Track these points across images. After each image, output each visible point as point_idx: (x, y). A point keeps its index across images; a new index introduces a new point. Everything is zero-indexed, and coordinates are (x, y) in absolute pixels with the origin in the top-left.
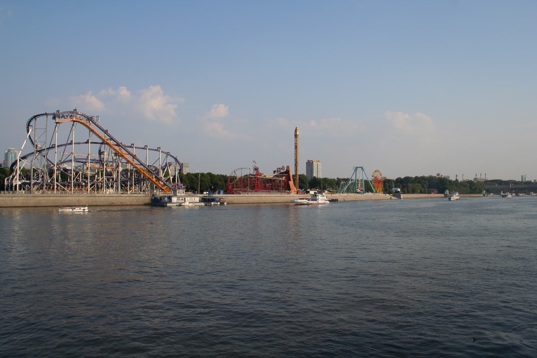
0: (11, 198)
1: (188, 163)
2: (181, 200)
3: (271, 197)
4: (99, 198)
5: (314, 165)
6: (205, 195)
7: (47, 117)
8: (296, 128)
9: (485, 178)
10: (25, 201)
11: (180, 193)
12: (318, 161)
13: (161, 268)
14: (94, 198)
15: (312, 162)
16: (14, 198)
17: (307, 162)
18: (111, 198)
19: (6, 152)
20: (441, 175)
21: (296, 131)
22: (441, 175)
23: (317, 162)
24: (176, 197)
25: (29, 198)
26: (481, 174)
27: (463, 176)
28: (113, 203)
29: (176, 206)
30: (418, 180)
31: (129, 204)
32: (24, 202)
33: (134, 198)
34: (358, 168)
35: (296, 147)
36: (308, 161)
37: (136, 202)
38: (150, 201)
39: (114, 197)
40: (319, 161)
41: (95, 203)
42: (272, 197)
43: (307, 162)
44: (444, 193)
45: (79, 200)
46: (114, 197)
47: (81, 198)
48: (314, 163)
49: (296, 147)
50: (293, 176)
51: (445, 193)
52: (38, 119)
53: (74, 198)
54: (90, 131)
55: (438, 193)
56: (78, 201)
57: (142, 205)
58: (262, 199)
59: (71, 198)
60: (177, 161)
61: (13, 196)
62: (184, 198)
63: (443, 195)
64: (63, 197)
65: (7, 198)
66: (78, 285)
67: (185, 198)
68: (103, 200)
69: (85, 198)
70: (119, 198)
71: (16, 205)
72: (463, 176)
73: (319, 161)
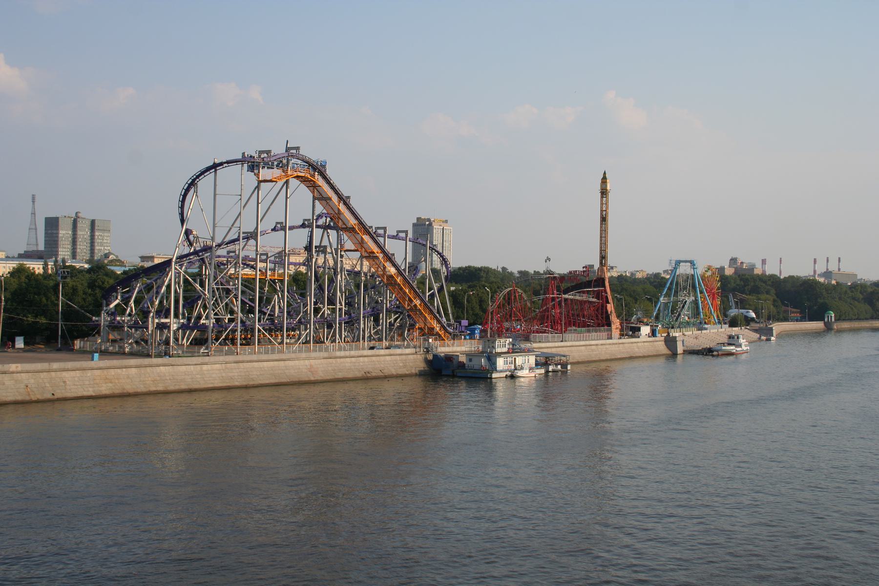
1: (110, 221)
3: (605, 347)
5: (434, 231)
8: (605, 173)
9: (839, 270)
10: (224, 375)
12: (443, 222)
13: (633, 520)
15: (430, 224)
16: (205, 367)
17: (415, 221)
20: (740, 262)
21: (604, 180)
22: (742, 263)
23: (442, 224)
25: (228, 365)
26: (828, 258)
27: (781, 263)
30: (752, 284)
32: (223, 377)
33: (398, 357)
34: (682, 264)
35: (604, 219)
36: (418, 219)
38: (425, 366)
39: (365, 356)
40: (446, 221)
41: (340, 374)
42: (607, 346)
43: (415, 221)
44: (824, 321)
45: (311, 366)
46: (365, 356)
47: (313, 362)
48: (436, 227)
49: (604, 219)
50: (316, 247)
51: (826, 320)
52: (221, 171)
53: (302, 362)
54: (314, 198)
55: (803, 319)
58: (593, 351)
59: (297, 362)
60: (446, 262)
61: (202, 361)
62: (513, 358)
63: (819, 325)
64: (284, 360)
66: (544, 568)
68: (349, 364)
69: (319, 361)
70: (374, 358)
71: (212, 383)
72: (781, 263)
73: (446, 221)
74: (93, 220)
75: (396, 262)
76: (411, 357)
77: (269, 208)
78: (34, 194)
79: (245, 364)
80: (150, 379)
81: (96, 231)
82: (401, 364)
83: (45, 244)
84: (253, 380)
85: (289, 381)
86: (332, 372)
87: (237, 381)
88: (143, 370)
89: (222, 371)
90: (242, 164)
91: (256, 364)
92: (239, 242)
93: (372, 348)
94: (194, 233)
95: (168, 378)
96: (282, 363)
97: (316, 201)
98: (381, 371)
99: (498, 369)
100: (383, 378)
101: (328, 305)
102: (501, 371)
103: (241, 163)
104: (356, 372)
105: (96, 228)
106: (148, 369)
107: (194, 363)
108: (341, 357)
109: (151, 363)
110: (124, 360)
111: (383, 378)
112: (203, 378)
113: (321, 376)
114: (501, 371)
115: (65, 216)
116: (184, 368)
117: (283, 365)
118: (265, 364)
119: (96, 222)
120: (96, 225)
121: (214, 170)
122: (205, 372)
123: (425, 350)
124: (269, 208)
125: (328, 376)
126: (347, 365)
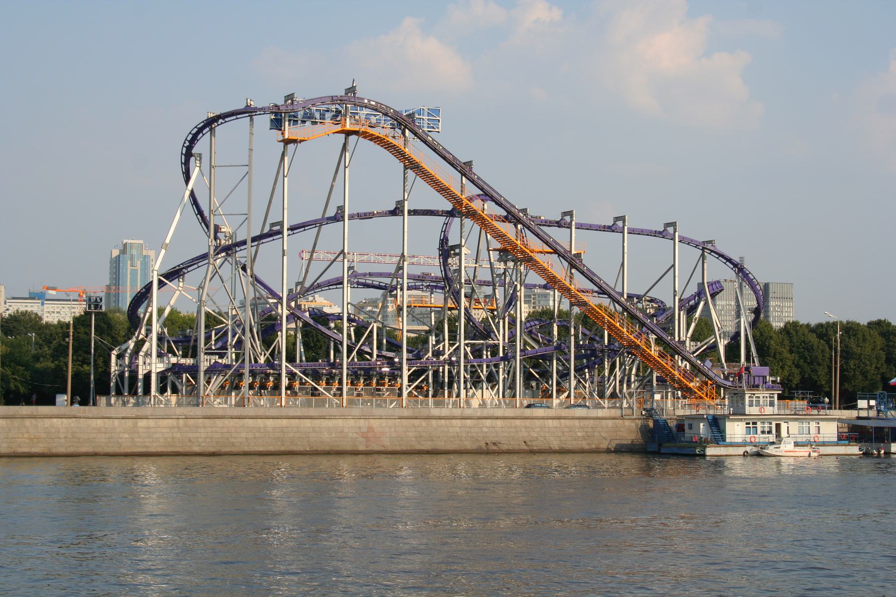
0: (130, 423)
2: (763, 432)
4: (443, 422)
6: (864, 414)
7: (252, 120)
11: (758, 404)
14: (424, 423)
16: (142, 423)
18: (488, 422)
19: (116, 253)
24: (741, 420)
28: (494, 444)
29: (744, 455)
31: (555, 445)
33: (577, 422)
37: (584, 438)
45: (370, 429)
46: (497, 418)
47: (375, 423)
52: (221, 129)
53: (351, 422)
54: (406, 168)
56: (365, 436)
57: (608, 451)
59: (340, 422)
65: (116, 422)
67: (778, 426)
68: (458, 430)
69: (390, 422)
70: (518, 422)
71: (146, 447)
74: (765, 283)
75: (584, 266)
76: (610, 423)
77: (332, 186)
78: (742, 256)
79: (226, 421)
80: (26, 435)
81: (770, 299)
82: (579, 434)
83: (824, 331)
84: (233, 445)
85: (308, 449)
86: (414, 439)
87: (199, 446)
88: (17, 423)
89: (176, 430)
90: (251, 116)
91: (250, 422)
92: (281, 236)
93: (529, 406)
94: (222, 230)
95: (62, 436)
96: (307, 423)
97: (409, 171)
98: (525, 442)
99: (728, 440)
100: (527, 452)
101: (465, 339)
102: (732, 445)
103: (247, 115)
104: (466, 443)
105: (771, 295)
106: (28, 422)
107: (121, 416)
108: (440, 418)
109: (35, 414)
110: (11, 407)
111: (527, 452)
112: (133, 438)
113: (383, 446)
114: (732, 445)
115: (726, 280)
116: (100, 422)
117: (309, 426)
118: (270, 423)
119: (771, 286)
120: (771, 290)
121: (207, 129)
122: (141, 430)
123: (644, 413)
124: (332, 186)
125: (400, 445)
126: (451, 430)
